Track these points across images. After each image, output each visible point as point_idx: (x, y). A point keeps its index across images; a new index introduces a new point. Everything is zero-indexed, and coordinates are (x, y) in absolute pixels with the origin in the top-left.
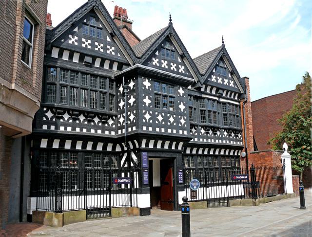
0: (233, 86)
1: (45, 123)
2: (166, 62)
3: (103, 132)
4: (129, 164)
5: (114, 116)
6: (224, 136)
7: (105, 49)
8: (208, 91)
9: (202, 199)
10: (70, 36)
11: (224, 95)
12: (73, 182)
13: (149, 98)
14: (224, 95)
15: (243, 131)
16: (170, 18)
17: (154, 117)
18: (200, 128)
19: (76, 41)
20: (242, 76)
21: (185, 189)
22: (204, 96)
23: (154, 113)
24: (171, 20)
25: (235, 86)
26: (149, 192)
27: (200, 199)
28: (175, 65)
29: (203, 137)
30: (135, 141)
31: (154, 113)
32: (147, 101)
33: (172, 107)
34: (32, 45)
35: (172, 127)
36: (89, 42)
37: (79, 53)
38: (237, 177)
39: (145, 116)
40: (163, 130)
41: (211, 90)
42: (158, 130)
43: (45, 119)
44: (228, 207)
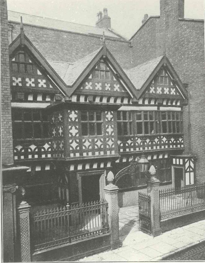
0: (175, 94)
2: (100, 84)
3: (135, 149)
5: (158, 136)
6: (162, 142)
7: (37, 83)
11: (165, 103)
12: (68, 210)
14: (165, 103)
17: (81, 144)
18: (162, 137)
25: (176, 93)
28: (20, 79)
31: (81, 140)
35: (100, 150)
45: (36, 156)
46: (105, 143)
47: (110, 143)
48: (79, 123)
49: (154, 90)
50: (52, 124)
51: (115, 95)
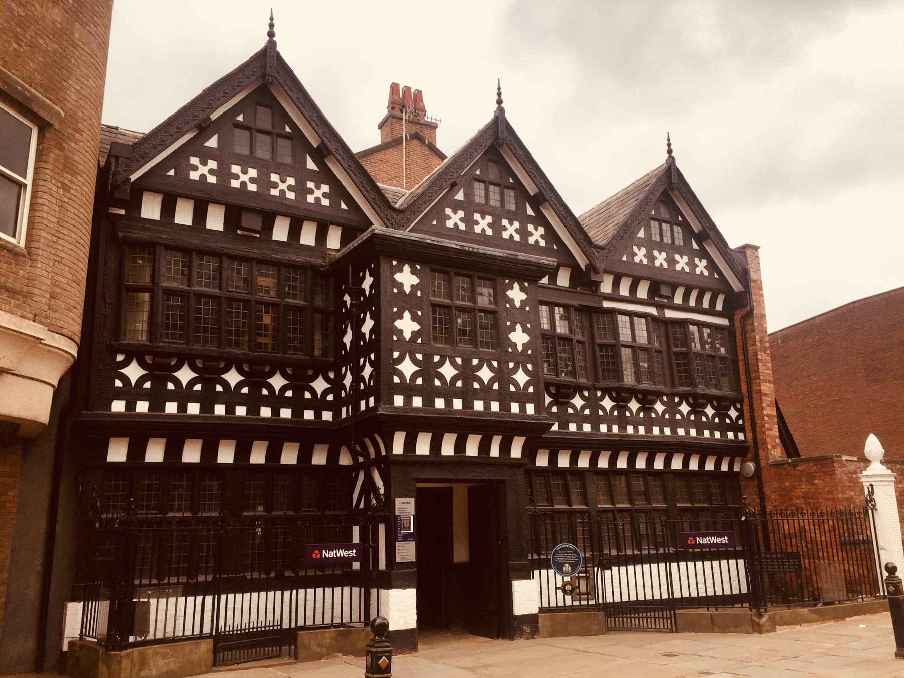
1: (118, 394)
4: (368, 501)
6: (678, 417)
7: (301, 190)
8: (624, 291)
9: (197, 631)
10: (195, 161)
13: (414, 318)
14: (678, 300)
15: (746, 400)
16: (499, 94)
17: (428, 370)
19: (211, 172)
20: (733, 243)
21: (537, 572)
22: (606, 305)
23: (428, 356)
24: (499, 102)
26: (415, 582)
27: (160, 636)
29: (609, 420)
30: (376, 436)
31: (428, 356)
32: (407, 326)
33: (726, 374)
34: (29, 181)
36: (291, 181)
37: (288, 216)
38: (699, 540)
39: (478, 373)
40: (457, 404)
41: (633, 289)
42: (440, 403)
43: (171, 386)
44: (675, 635)
45: (241, 411)
46: (503, 376)
47: (521, 377)
48: (450, 411)
49: (697, 266)
50: (278, 367)
51: (635, 274)
